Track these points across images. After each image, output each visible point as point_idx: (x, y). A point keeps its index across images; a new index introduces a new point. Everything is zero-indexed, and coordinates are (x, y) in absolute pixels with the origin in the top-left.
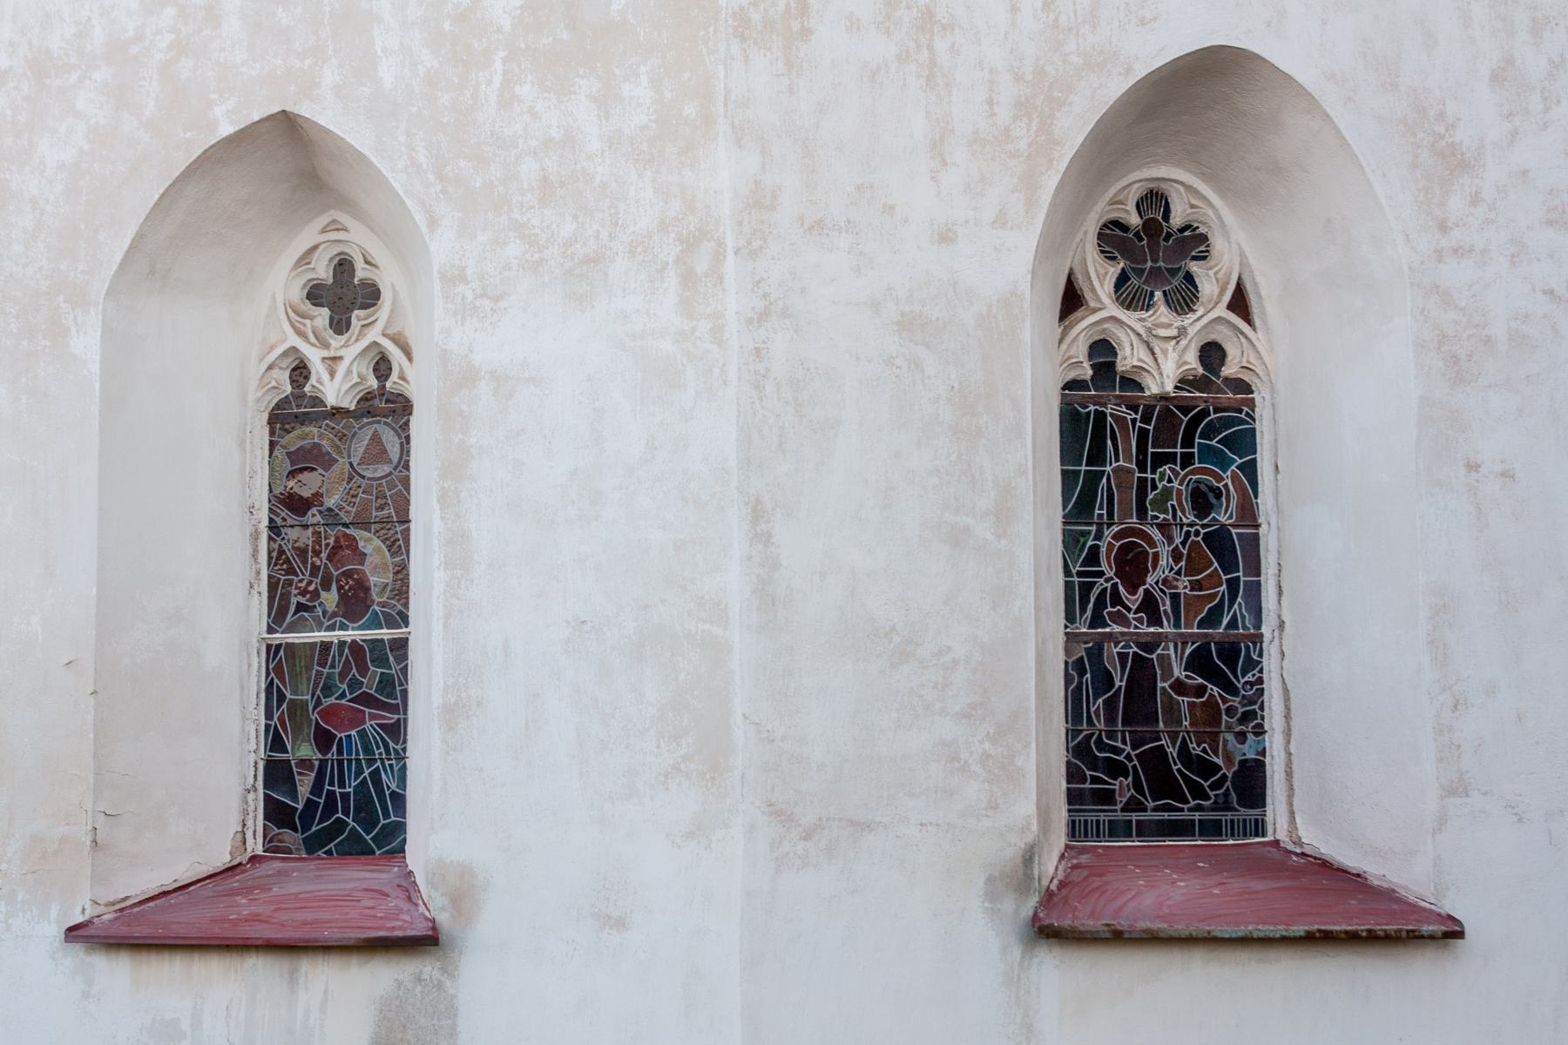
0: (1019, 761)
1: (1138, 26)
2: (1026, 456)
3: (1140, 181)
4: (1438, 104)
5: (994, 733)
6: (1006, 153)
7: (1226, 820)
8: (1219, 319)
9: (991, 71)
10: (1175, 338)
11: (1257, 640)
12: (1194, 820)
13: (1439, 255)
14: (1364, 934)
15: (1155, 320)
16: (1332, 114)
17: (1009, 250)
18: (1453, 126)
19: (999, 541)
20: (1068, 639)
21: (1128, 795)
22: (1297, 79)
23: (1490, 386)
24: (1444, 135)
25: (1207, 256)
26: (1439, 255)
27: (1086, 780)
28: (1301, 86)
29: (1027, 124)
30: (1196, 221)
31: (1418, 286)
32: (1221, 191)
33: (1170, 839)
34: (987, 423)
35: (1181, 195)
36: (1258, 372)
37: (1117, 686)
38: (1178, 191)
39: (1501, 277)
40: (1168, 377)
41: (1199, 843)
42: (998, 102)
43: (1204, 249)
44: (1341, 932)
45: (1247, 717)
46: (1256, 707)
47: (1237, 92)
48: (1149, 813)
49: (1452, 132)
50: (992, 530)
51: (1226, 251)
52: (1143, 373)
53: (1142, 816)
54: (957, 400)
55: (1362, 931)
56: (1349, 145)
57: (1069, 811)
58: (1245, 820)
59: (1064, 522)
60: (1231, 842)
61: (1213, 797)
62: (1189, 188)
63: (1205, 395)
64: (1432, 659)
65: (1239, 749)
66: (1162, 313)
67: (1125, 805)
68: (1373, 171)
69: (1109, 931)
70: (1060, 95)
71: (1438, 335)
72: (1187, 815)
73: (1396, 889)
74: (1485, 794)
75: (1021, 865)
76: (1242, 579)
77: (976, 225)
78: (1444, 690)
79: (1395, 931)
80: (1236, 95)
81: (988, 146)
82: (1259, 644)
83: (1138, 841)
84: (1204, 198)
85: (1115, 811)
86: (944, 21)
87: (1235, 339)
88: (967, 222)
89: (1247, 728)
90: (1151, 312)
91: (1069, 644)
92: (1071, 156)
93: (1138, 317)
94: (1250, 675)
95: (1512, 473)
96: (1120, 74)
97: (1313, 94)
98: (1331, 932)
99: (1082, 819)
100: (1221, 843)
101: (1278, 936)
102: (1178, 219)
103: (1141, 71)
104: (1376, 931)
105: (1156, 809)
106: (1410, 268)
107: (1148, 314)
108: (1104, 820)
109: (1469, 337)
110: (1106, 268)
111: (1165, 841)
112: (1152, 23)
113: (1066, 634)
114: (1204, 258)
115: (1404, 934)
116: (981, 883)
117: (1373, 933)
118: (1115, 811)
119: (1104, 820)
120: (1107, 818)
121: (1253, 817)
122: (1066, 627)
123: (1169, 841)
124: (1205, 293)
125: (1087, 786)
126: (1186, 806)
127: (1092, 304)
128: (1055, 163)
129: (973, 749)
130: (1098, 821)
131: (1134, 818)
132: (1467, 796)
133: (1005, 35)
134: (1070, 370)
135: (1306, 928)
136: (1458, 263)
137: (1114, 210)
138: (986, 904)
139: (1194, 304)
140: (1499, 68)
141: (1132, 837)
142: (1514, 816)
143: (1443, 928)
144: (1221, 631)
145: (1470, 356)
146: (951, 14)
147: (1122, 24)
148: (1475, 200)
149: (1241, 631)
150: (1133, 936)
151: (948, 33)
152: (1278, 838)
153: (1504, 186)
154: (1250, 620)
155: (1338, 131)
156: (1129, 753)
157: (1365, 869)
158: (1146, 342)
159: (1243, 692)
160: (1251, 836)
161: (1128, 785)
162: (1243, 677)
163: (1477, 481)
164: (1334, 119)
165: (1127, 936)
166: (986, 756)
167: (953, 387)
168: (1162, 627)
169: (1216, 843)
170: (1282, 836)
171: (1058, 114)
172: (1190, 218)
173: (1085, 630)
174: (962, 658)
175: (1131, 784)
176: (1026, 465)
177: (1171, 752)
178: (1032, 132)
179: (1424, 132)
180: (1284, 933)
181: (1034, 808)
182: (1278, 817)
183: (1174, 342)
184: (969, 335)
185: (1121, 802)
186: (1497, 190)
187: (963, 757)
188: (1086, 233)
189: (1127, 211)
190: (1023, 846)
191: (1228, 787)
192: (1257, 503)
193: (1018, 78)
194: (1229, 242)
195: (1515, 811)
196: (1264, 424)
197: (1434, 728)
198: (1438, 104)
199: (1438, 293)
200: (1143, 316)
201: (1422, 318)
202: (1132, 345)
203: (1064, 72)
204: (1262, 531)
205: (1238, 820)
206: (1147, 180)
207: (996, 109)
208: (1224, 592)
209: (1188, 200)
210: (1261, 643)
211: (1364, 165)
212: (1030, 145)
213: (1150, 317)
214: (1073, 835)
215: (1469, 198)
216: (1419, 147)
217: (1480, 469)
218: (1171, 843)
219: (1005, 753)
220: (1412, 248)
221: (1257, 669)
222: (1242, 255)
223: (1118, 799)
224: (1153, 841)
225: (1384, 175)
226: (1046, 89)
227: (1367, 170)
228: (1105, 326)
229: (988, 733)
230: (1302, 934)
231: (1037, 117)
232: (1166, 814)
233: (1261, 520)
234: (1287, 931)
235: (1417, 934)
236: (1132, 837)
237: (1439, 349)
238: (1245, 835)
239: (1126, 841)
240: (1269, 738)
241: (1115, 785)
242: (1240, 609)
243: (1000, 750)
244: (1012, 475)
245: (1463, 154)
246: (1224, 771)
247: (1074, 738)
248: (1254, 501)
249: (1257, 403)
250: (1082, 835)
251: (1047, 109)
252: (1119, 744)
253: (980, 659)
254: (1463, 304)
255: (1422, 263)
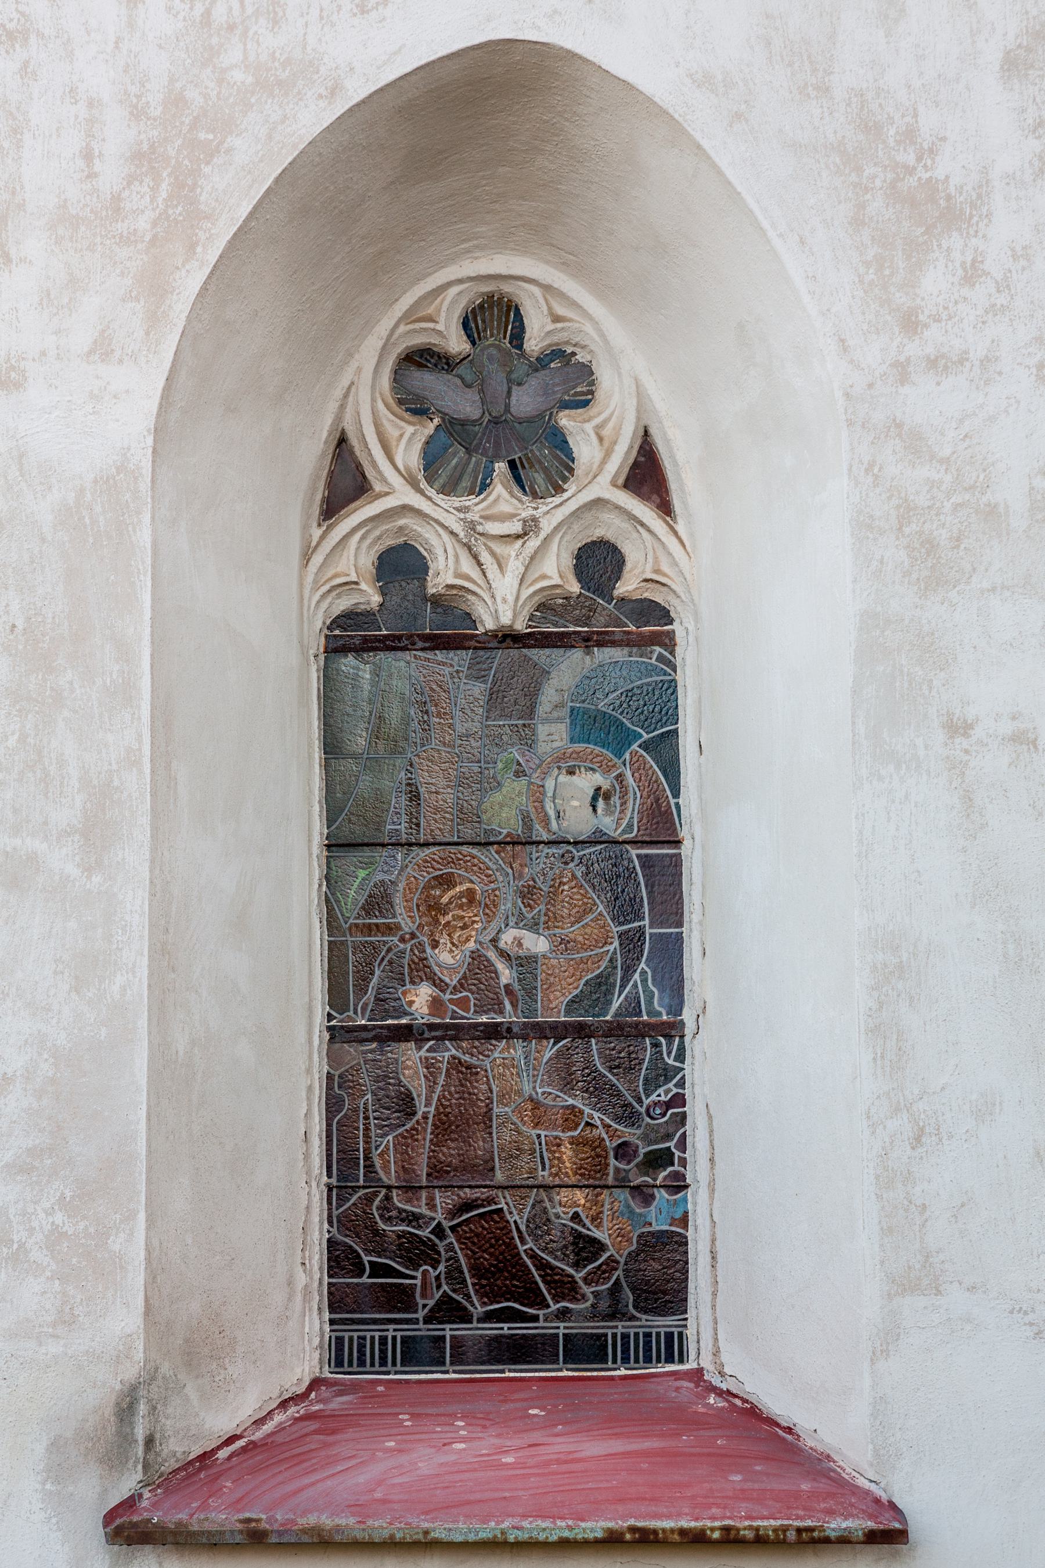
0: (116, 1243)
1: (355, 15)
2: (140, 736)
3: (460, 281)
4: (903, 116)
5: (72, 1197)
6: (114, 237)
7: (614, 1336)
8: (599, 503)
9: (90, 104)
10: (518, 537)
11: (673, 1033)
12: (557, 1335)
13: (902, 372)
14: (716, 1535)
15: (488, 507)
16: (705, 143)
17: (115, 397)
18: (931, 151)
19: (89, 877)
20: (332, 1038)
21: (437, 1296)
22: (640, 88)
23: (993, 589)
24: (914, 168)
25: (590, 400)
26: (902, 372)
27: (364, 1271)
28: (649, 100)
29: (152, 189)
30: (567, 343)
31: (863, 426)
32: (602, 290)
33: (513, 1367)
34: (71, 683)
35: (537, 302)
36: (673, 586)
37: (420, 1114)
38: (532, 296)
39: (1018, 402)
40: (504, 601)
41: (565, 1373)
42: (101, 155)
43: (584, 389)
44: (672, 1531)
45: (659, 1160)
46: (671, 1144)
47: (567, 120)
48: (475, 1325)
49: (929, 162)
50: (77, 858)
51: (617, 389)
52: (469, 597)
53: (462, 1330)
54: (20, 647)
55: (713, 1529)
56: (739, 194)
57: (332, 1322)
58: (647, 1335)
59: (328, 846)
60: (623, 1372)
61: (591, 1297)
62: (547, 288)
63: (586, 629)
64: (874, 1059)
65: (641, 1215)
66: (499, 497)
67: (431, 1311)
68: (781, 235)
69: (241, 1532)
70: (211, 136)
71: (898, 507)
72: (345, 1331)
73: (832, 1455)
74: (971, 1289)
75: (112, 1419)
76: (648, 931)
77: (58, 357)
78: (897, 1110)
79: (775, 1530)
80: (567, 124)
81: (83, 228)
82: (677, 1039)
83: (455, 1372)
84: (574, 304)
85: (416, 1321)
86: (10, 26)
87: (635, 535)
88: (43, 354)
89: (655, 1180)
90: (482, 496)
91: (337, 1046)
92: (229, 237)
93: (457, 504)
94: (661, 1091)
95: (1031, 736)
96: (320, 96)
97: (671, 111)
98: (655, 1532)
99: (355, 1335)
100: (603, 1373)
101: (554, 1538)
102: (533, 342)
103: (357, 90)
104: (738, 1530)
105: (488, 1317)
106: (847, 395)
107: (477, 500)
108: (394, 1338)
109: (956, 507)
110: (402, 428)
111: (503, 1371)
112: (380, 8)
113: (330, 1029)
114: (585, 404)
115: (792, 1535)
116: (40, 1449)
117: (733, 1532)
118: (416, 1321)
119: (394, 1338)
120: (399, 1334)
121: (662, 1330)
122: (330, 1017)
123: (510, 1371)
124: (582, 461)
125: (365, 1279)
126: (541, 1313)
127: (378, 487)
128: (199, 249)
129: (35, 1224)
130: (383, 1341)
131: (448, 1334)
132: (939, 1293)
133: (116, 43)
134: (339, 596)
135: (610, 1525)
136: (938, 384)
137: (415, 331)
138: (48, 1486)
139: (565, 480)
140: (1020, 46)
141: (443, 1364)
142: (1028, 1327)
143: (870, 1524)
144: (608, 1018)
145: (958, 539)
146: (22, 14)
147: (325, 14)
148: (972, 273)
149: (645, 1018)
150: (285, 1539)
151: (17, 46)
152: (702, 1365)
153: (1024, 248)
154: (661, 999)
155: (719, 172)
156: (439, 1224)
157: (796, 1421)
158: (465, 545)
159: (648, 1120)
160: (659, 1361)
161: (438, 1278)
162: (648, 1096)
163: (966, 752)
164: (712, 153)
165: (273, 1539)
166: (56, 1236)
167: (14, 626)
168: (501, 1012)
169: (595, 1374)
170: (706, 1362)
171: (207, 170)
172: (555, 339)
173: (363, 1022)
174: (18, 1074)
175: (443, 1276)
176: (140, 750)
177: (515, 1222)
178: (160, 200)
179: (875, 164)
180: (566, 1534)
181: (139, 1321)
182: (702, 1330)
183: (520, 542)
184: (43, 540)
185: (424, 1306)
186: (1013, 256)
187: (16, 1238)
188: (359, 370)
189: (439, 333)
190: (118, 1387)
191: (618, 1279)
192: (677, 805)
193: (137, 113)
194: (620, 375)
195: (1030, 1317)
196: (687, 672)
197: (877, 1177)
198: (903, 116)
199: (900, 435)
200: (468, 503)
201: (870, 479)
202: (446, 551)
203: (219, 99)
204: (685, 849)
205: (636, 1334)
206: (471, 279)
207: (98, 166)
208: (615, 952)
209: (550, 308)
210: (682, 1037)
211: (765, 224)
212: (155, 224)
213: (477, 504)
214: (339, 1363)
215: (960, 272)
216: (867, 190)
217: (972, 732)
218: (512, 1375)
219: (92, 1230)
220: (852, 361)
221: (675, 1081)
222: (641, 395)
223: (421, 1302)
224: (536, 1371)
225: (802, 242)
226: (185, 129)
227: (771, 234)
228: (402, 522)
229: (63, 1197)
230: (599, 1535)
231: (169, 175)
232: (506, 1326)
233: (684, 833)
234: (570, 1528)
235: (816, 1534)
236: (443, 1364)
237: (900, 529)
238: (648, 1360)
239: (432, 1372)
240: (693, 1195)
241: (414, 1278)
242: (644, 981)
243: (81, 1226)
244: (115, 767)
245: (949, 198)
246: (612, 1251)
247: (341, 1200)
248: (672, 801)
249: (678, 640)
250: (377, 1364)
251: (186, 162)
252: (424, 1210)
253: (50, 1074)
254: (947, 451)
255: (870, 386)
